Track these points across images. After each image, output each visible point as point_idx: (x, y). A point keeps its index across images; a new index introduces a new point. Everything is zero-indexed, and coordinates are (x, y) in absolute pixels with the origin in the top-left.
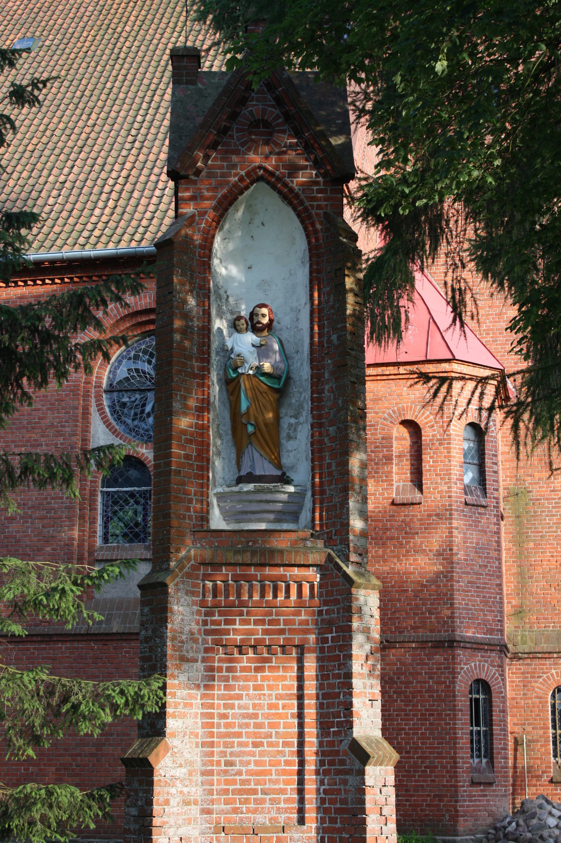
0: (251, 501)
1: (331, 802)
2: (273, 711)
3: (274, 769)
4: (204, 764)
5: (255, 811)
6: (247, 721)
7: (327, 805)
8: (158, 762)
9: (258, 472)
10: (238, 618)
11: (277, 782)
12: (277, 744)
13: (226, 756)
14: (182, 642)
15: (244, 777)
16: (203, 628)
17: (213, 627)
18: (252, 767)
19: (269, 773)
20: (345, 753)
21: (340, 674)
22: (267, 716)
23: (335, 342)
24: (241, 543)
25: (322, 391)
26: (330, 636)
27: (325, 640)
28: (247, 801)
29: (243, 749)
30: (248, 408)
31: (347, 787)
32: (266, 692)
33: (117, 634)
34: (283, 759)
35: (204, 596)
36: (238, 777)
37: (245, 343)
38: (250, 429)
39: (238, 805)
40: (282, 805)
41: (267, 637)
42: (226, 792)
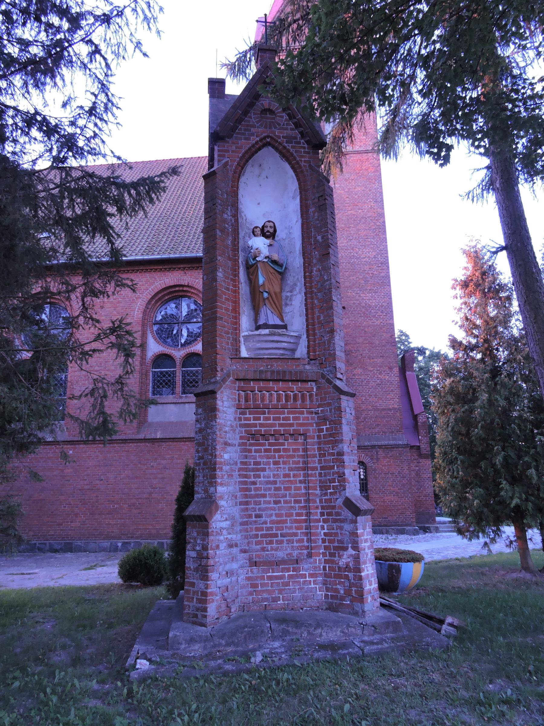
0: (266, 341)
1: (330, 541)
2: (287, 479)
3: (288, 519)
4: (242, 517)
5: (277, 549)
6: (269, 486)
7: (327, 544)
8: (211, 517)
9: (271, 322)
10: (262, 416)
11: (291, 528)
12: (290, 502)
13: (255, 511)
14: (226, 432)
15: (268, 525)
16: (238, 423)
17: (246, 422)
18: (274, 518)
19: (285, 522)
20: (340, 508)
21: (334, 453)
22: (283, 483)
23: (320, 240)
24: (263, 366)
25: (311, 272)
26: (324, 427)
27: (321, 430)
28: (271, 542)
29: (267, 506)
30: (264, 282)
31: (343, 532)
32: (282, 466)
33: (159, 439)
34: (294, 512)
35: (239, 401)
36: (264, 526)
37: (260, 243)
38: (266, 295)
39: (265, 545)
40: (295, 544)
41: (282, 429)
42: (256, 536)
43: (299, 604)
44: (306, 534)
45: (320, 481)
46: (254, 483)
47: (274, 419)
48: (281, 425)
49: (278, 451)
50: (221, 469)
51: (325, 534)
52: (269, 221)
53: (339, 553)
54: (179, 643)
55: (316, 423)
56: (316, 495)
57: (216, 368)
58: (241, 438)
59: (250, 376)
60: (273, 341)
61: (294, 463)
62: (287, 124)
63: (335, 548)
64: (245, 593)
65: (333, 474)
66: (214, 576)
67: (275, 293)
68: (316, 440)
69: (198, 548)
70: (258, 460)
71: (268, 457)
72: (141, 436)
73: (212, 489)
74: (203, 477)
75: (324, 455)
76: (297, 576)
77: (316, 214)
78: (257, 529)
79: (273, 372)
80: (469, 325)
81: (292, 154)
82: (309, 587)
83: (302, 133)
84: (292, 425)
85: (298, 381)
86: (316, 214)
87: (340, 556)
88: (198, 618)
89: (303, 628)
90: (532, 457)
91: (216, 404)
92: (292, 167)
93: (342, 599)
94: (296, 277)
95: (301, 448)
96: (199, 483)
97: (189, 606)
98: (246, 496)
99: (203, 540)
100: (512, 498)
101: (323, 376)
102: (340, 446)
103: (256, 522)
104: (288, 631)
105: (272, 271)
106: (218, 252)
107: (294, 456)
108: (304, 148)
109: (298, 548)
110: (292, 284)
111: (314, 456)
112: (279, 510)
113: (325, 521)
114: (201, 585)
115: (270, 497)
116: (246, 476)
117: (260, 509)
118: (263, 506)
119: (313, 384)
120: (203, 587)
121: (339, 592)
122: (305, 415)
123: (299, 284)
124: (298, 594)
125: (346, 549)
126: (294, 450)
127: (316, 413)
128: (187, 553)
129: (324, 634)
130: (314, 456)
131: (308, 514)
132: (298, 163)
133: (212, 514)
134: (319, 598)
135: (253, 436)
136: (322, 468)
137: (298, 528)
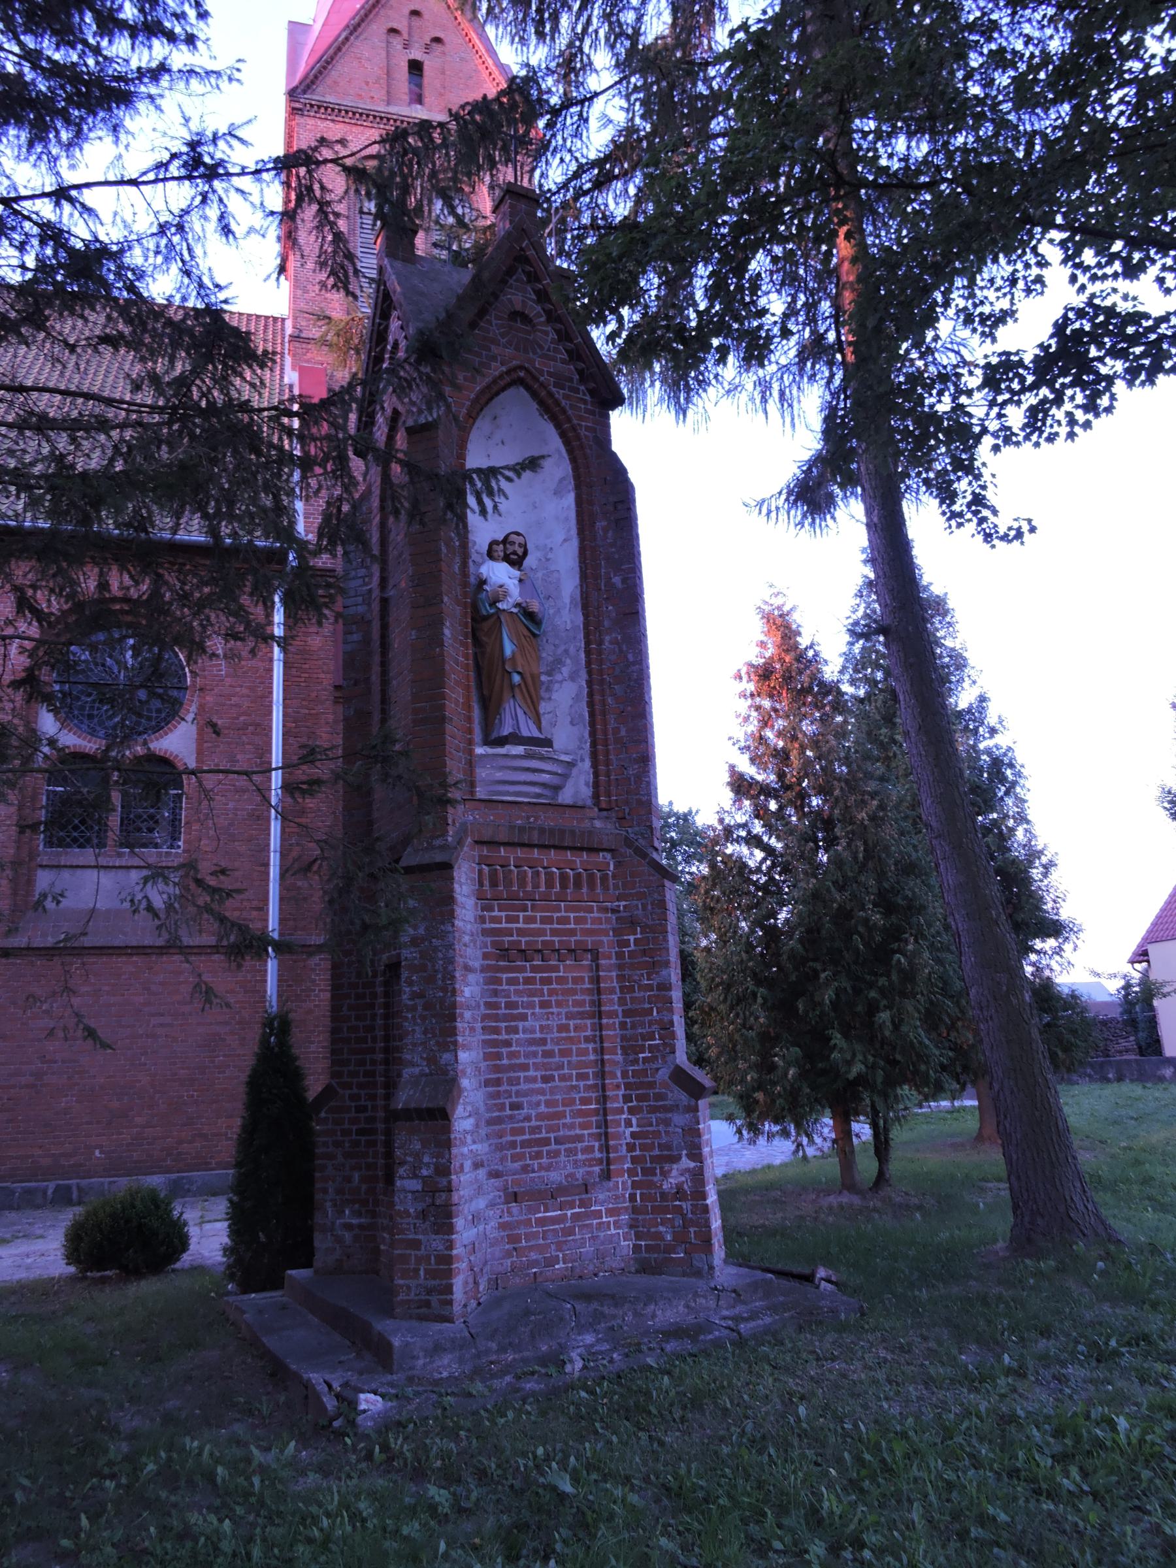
0: (516, 769)
5: (548, 1168)
6: (534, 1048)
9: (525, 733)
11: (572, 1126)
12: (570, 1078)
15: (534, 1123)
18: (542, 1109)
19: (562, 1115)
22: (557, 1041)
23: (620, 585)
25: (601, 643)
26: (632, 938)
28: (538, 1155)
30: (513, 653)
32: (555, 1010)
37: (499, 573)
40: (580, 1156)
41: (556, 939)
42: (513, 1144)
43: (591, 1267)
44: (598, 1137)
45: (623, 1038)
46: (508, 1043)
47: (544, 920)
48: (554, 932)
49: (548, 981)
50: (462, 1015)
51: (633, 1135)
52: (518, 534)
53: (661, 1168)
54: (413, 1357)
55: (614, 930)
56: (616, 1063)
57: (446, 819)
58: (486, 956)
59: (502, 837)
60: (528, 769)
61: (577, 1003)
62: (556, 350)
63: (654, 1159)
64: (498, 1254)
65: (651, 1023)
66: (459, 1222)
67: (532, 676)
68: (614, 961)
69: (425, 1172)
70: (513, 999)
71: (532, 994)
72: (19, 941)
73: (446, 1057)
74: (425, 1033)
75: (631, 989)
76: (588, 1215)
77: (610, 534)
78: (515, 1132)
79: (542, 831)
80: (758, 749)
81: (564, 411)
82: (606, 1233)
83: (580, 372)
84: (572, 932)
85: (581, 849)
86: (610, 534)
87: (665, 1174)
88: (433, 1305)
89: (627, 1306)
90: (882, 991)
91: (452, 890)
92: (563, 435)
93: (670, 1249)
94: (563, 648)
95: (586, 975)
96: (414, 1045)
97: (409, 1287)
98: (497, 1069)
99: (439, 1155)
100: (849, 1063)
101: (628, 842)
102: (664, 973)
103: (511, 1117)
104: (602, 1313)
105: (527, 633)
106: (444, 588)
107: (573, 992)
108: (585, 402)
109: (585, 1163)
110: (551, 659)
111: (612, 991)
112: (552, 1093)
113: (631, 1111)
114: (436, 1243)
115: (536, 1070)
116: (496, 1030)
117: (518, 1094)
118: (523, 1086)
119: (608, 856)
120: (441, 1247)
121: (663, 1239)
122: (596, 915)
123: (568, 661)
124: (588, 1249)
125: (676, 1159)
126: (576, 980)
127: (614, 911)
128: (398, 1183)
129: (659, 1313)
130: (612, 991)
131: (604, 1099)
132: (574, 428)
133: (454, 1104)
134: (625, 1252)
135: (505, 954)
136: (626, 1014)
137: (583, 1126)
